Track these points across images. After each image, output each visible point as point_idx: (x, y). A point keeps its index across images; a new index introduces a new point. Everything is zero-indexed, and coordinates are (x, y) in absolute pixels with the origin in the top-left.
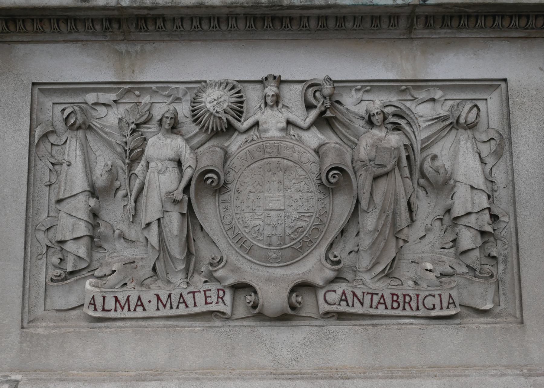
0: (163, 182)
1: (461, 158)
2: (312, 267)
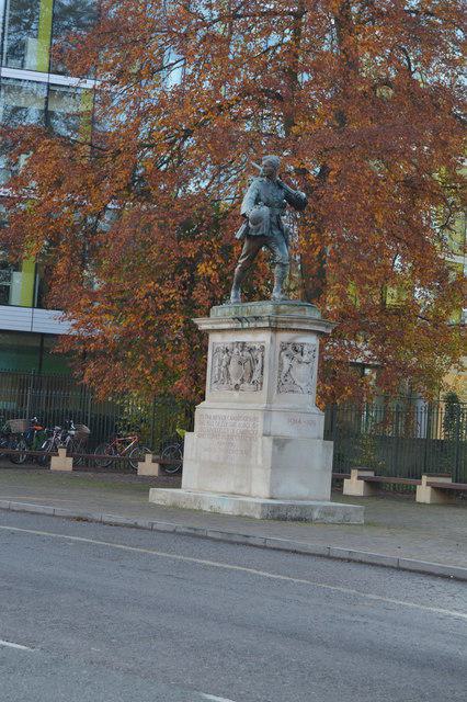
0: (224, 363)
1: (259, 357)
2: (239, 382)
